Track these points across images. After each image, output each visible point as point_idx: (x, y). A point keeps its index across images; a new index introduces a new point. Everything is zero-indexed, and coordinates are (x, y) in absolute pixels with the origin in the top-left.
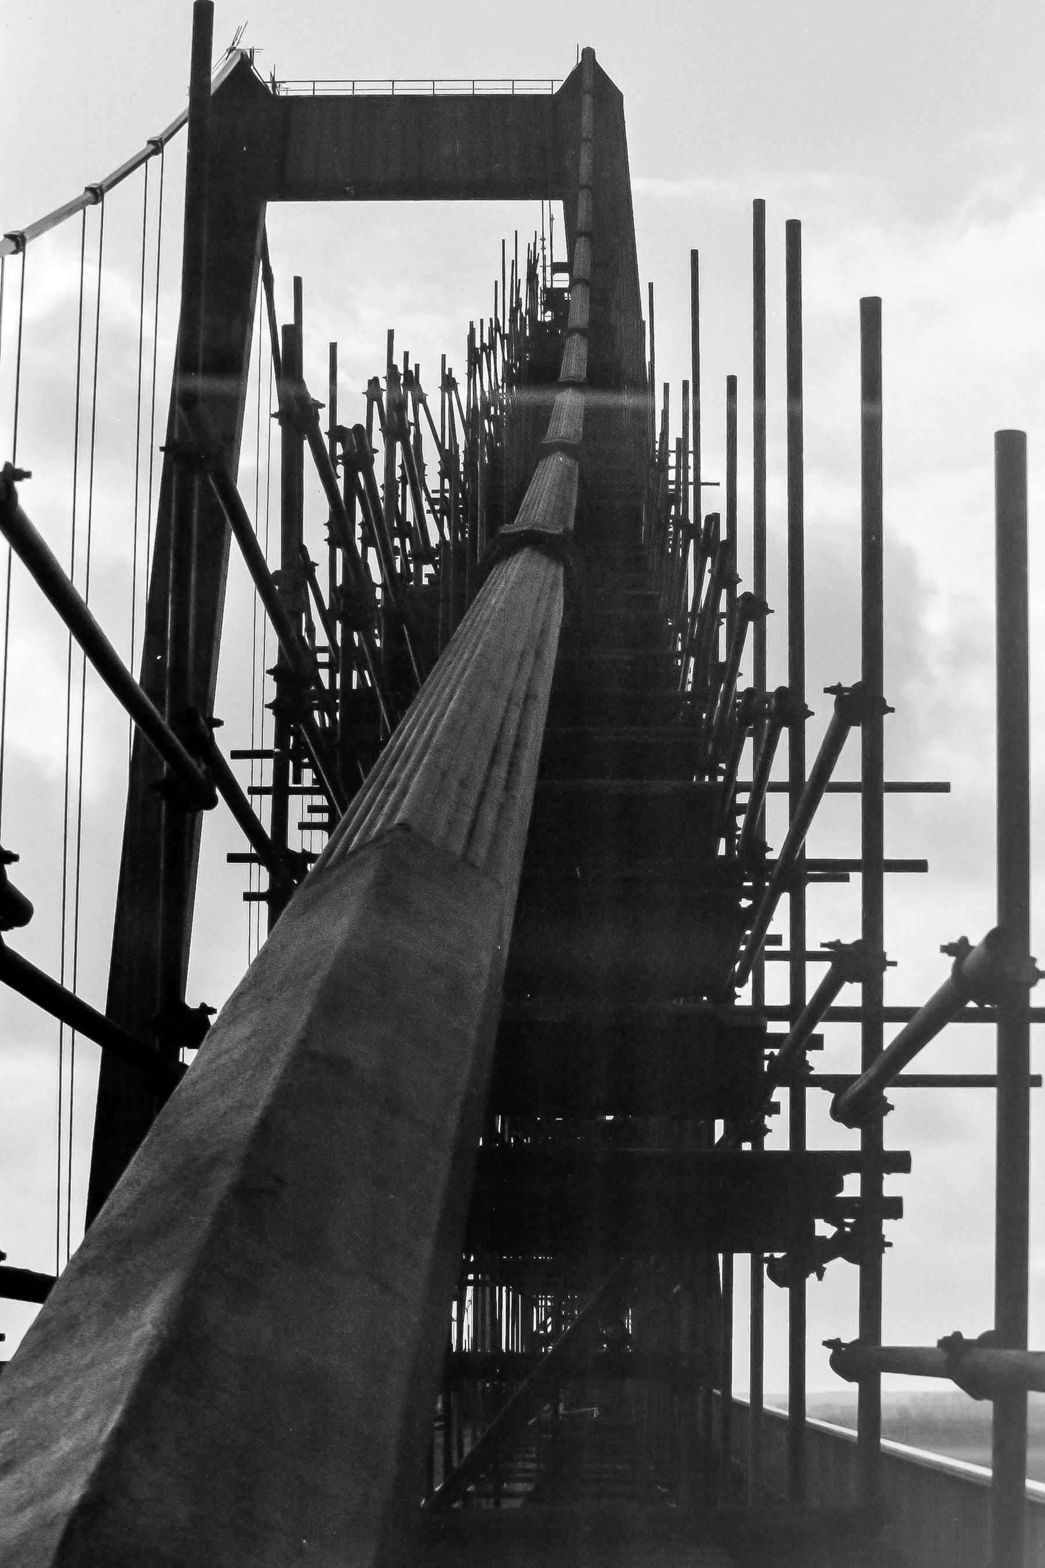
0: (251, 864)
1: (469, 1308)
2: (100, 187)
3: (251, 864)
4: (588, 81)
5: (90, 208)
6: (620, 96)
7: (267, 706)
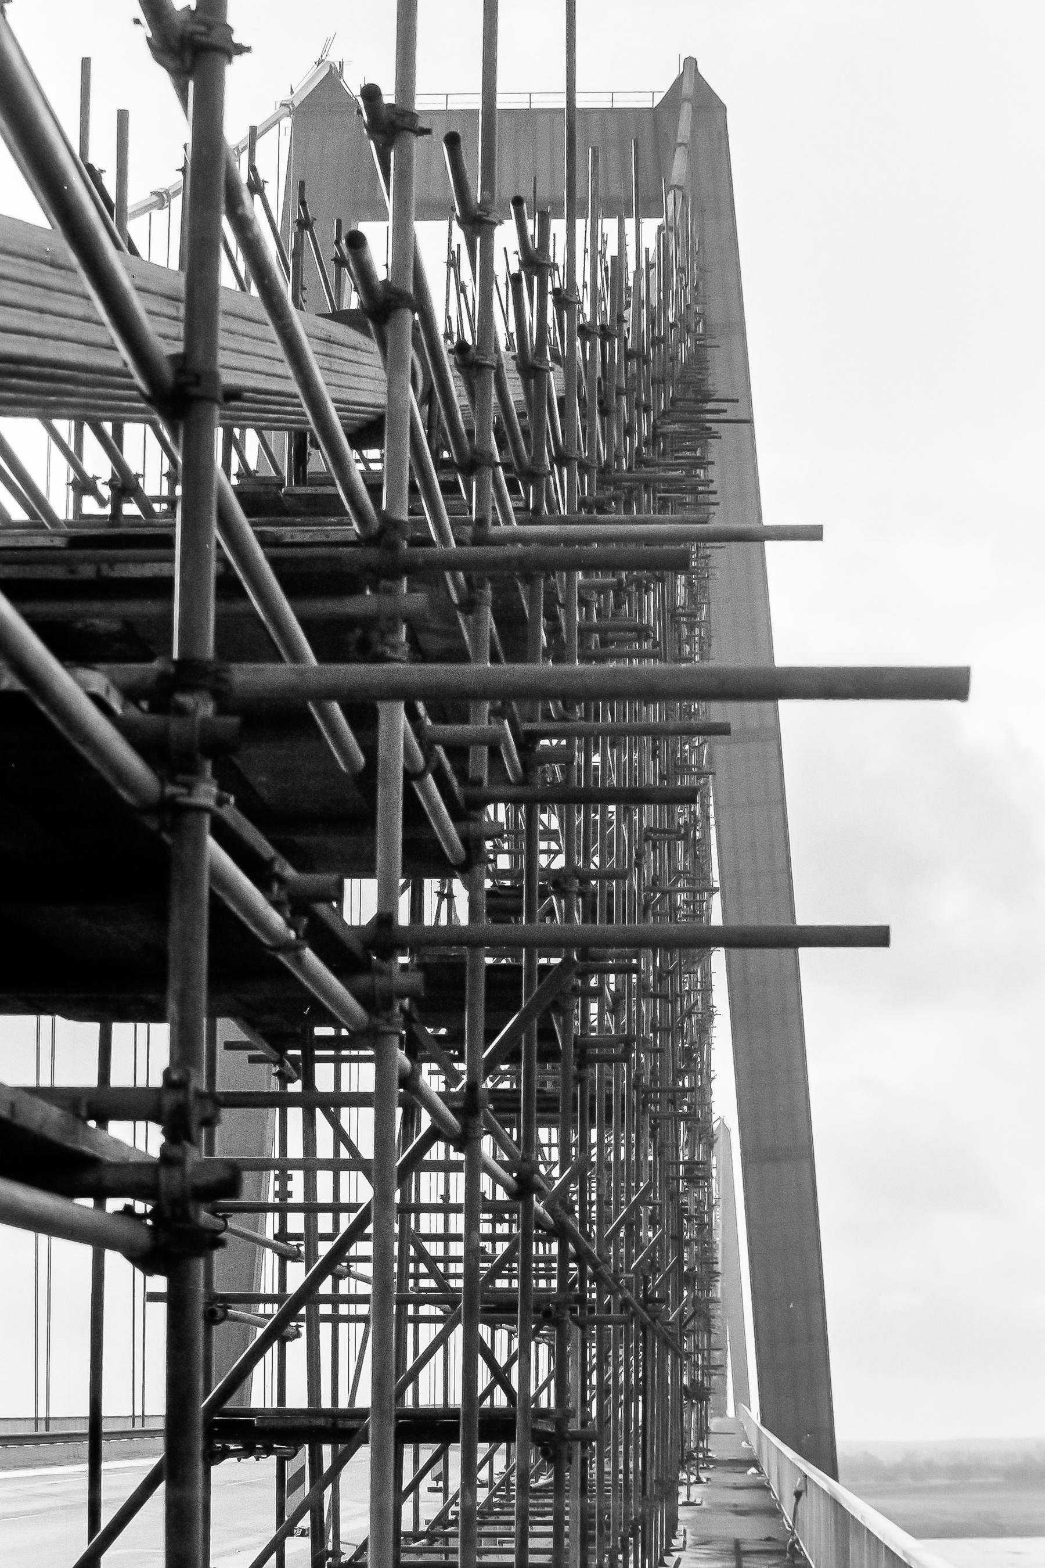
0: (135, 1085)
1: (640, 1404)
2: (167, 192)
3: (135, 1085)
4: (687, 89)
5: (155, 212)
6: (723, 108)
7: (164, 475)
